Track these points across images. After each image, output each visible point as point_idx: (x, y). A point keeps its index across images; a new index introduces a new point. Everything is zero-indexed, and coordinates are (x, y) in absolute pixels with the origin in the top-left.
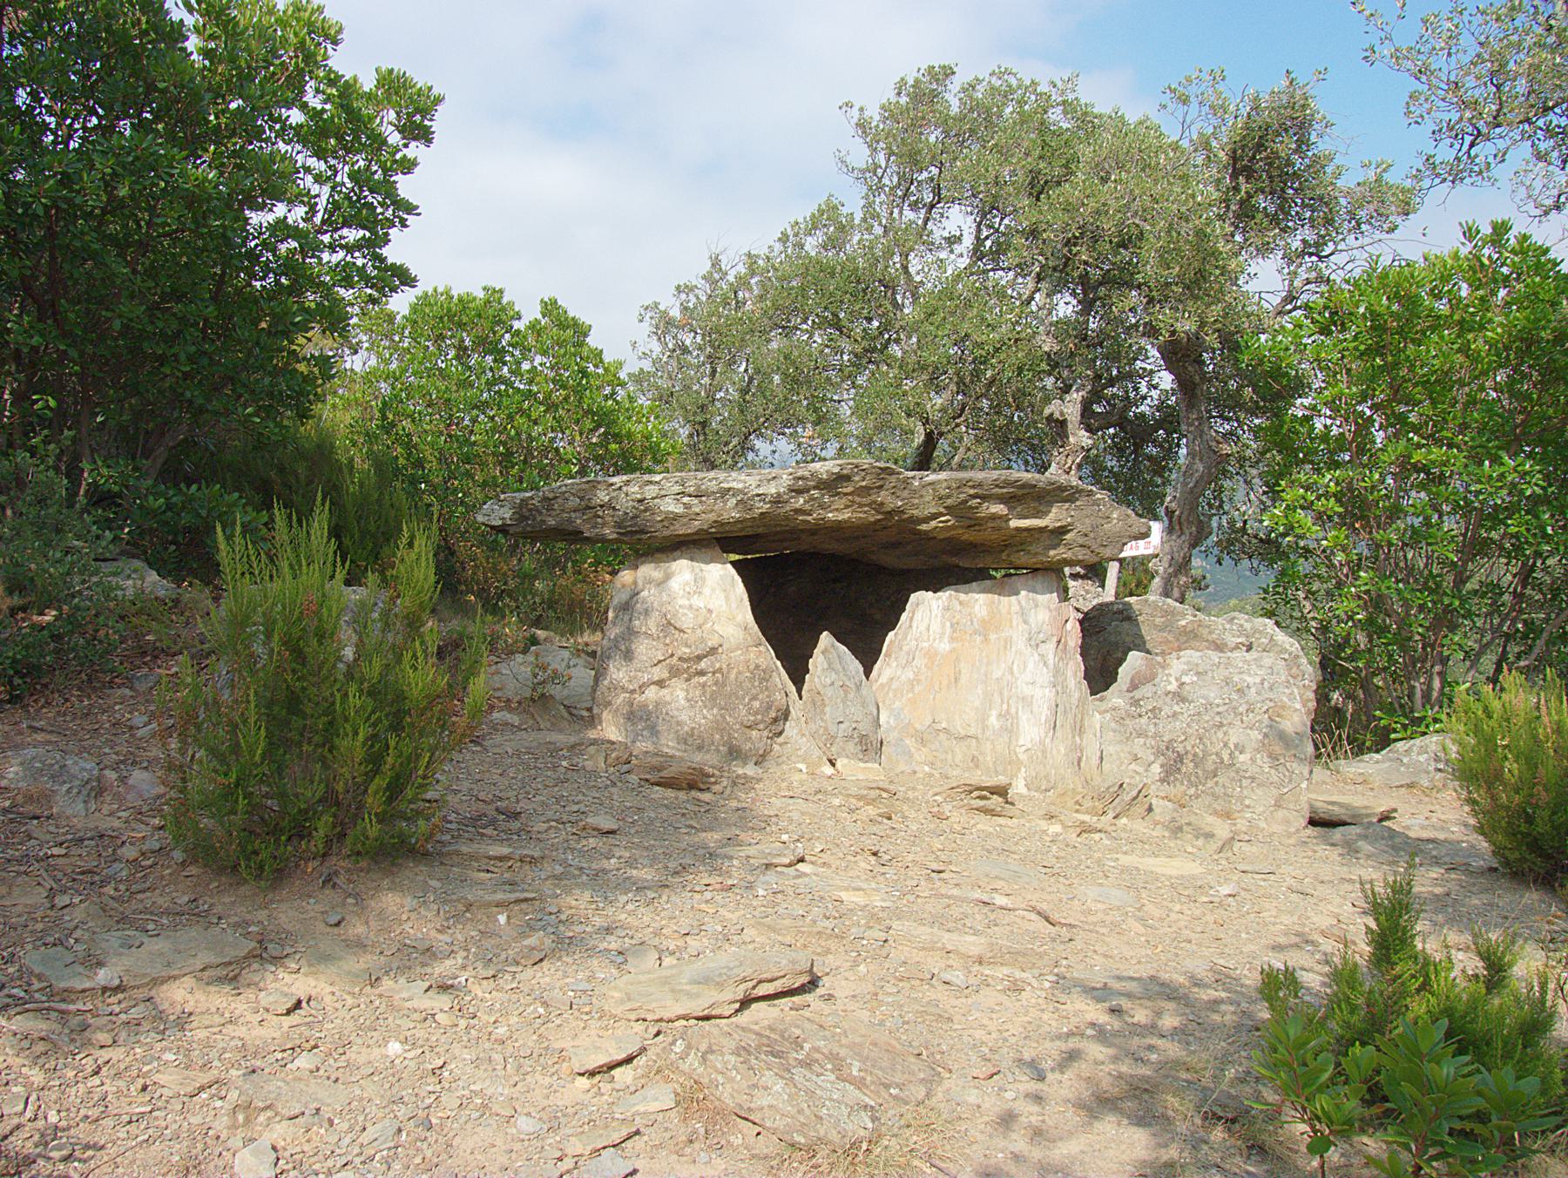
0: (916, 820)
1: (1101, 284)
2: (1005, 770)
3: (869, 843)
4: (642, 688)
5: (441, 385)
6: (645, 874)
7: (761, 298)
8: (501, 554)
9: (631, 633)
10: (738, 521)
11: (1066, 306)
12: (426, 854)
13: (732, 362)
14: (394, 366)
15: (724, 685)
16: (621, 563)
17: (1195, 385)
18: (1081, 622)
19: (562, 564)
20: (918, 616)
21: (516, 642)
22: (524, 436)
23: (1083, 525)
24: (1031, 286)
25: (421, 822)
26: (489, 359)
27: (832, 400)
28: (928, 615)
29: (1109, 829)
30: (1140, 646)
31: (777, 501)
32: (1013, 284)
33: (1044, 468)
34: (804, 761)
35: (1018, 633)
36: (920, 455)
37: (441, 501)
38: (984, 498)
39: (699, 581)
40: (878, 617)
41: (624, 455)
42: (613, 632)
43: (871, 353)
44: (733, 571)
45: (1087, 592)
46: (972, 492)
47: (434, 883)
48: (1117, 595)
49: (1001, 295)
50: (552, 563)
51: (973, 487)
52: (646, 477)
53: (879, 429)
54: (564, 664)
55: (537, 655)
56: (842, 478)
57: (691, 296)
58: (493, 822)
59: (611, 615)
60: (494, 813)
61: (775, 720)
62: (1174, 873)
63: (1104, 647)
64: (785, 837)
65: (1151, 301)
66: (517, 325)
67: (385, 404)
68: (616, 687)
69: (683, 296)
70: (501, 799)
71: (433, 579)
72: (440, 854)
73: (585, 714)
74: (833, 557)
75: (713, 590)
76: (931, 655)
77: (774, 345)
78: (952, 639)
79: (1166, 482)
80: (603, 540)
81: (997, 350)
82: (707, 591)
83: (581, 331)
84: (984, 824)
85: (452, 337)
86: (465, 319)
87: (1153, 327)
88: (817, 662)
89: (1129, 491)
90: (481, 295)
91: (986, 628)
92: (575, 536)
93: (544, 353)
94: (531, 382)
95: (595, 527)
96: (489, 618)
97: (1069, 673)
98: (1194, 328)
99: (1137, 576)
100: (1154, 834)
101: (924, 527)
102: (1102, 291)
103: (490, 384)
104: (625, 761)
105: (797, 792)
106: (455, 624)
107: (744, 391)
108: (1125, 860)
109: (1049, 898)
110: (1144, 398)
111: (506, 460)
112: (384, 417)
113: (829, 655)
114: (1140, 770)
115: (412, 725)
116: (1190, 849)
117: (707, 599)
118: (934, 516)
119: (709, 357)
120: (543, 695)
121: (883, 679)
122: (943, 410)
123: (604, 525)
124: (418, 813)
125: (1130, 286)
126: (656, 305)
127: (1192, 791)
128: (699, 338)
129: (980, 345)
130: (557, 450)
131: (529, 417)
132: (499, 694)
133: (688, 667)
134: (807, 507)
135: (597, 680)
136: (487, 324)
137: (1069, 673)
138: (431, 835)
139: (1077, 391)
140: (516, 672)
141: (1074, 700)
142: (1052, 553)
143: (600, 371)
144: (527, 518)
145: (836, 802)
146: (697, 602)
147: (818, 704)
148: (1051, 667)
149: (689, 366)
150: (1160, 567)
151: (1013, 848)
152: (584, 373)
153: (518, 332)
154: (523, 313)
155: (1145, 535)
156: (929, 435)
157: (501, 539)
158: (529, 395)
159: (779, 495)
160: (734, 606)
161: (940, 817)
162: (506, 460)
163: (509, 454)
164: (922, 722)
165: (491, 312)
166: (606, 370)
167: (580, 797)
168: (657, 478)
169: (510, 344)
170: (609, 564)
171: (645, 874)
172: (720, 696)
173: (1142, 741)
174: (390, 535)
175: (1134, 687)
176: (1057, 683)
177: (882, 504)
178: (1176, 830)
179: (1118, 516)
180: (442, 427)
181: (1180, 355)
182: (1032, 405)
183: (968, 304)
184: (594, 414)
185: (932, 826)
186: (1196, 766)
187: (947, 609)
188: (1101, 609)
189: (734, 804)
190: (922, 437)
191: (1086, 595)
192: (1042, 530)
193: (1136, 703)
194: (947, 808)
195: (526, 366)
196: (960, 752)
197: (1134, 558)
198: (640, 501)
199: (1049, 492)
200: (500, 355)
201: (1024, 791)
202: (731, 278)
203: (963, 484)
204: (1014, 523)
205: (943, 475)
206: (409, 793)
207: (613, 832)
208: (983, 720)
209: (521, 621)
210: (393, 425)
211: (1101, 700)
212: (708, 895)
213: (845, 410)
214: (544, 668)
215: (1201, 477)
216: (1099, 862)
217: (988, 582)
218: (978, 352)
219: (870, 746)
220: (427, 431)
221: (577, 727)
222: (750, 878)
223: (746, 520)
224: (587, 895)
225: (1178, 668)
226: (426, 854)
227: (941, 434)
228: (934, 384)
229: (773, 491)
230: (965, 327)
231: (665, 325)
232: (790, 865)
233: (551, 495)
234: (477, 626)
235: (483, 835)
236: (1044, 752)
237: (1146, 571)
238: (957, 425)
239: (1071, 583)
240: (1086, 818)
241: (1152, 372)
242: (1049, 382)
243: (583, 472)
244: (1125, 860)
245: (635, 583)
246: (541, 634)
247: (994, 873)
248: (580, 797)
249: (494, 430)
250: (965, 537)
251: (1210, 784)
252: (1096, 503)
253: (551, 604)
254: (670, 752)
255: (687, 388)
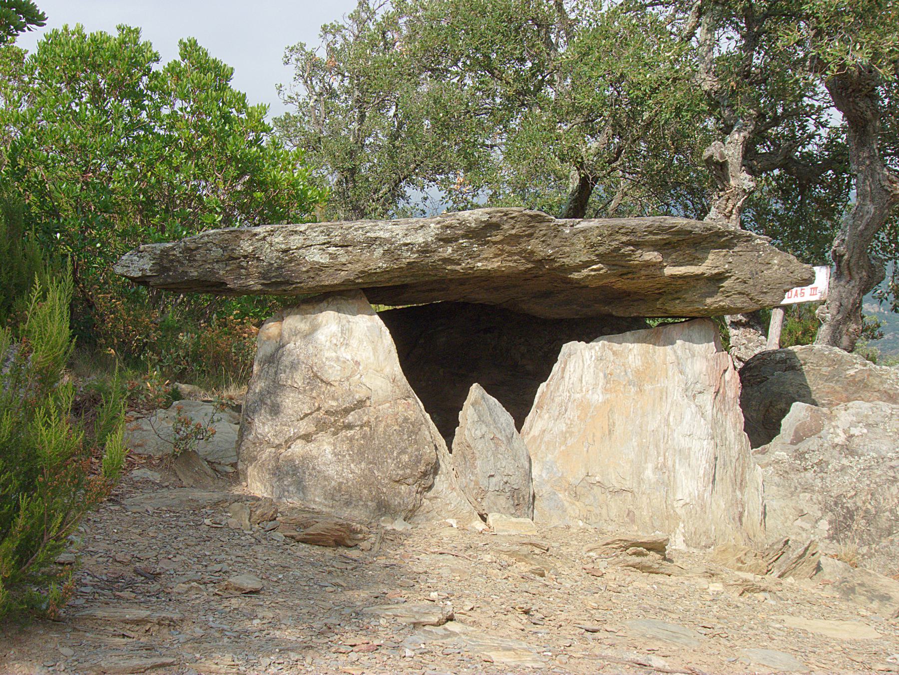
0: (570, 577)
1: (766, 16)
2: (662, 526)
3: (521, 600)
4: (288, 442)
5: (76, 130)
6: (290, 635)
7: (410, 39)
8: (142, 306)
9: (276, 387)
10: (386, 272)
11: (728, 41)
12: (58, 620)
13: (381, 106)
14: (24, 108)
15: (372, 438)
16: (268, 314)
17: (867, 122)
18: (741, 372)
19: (204, 316)
20: (570, 367)
21: (157, 397)
22: (165, 184)
23: (741, 271)
24: (692, 20)
25: (53, 587)
26: (127, 103)
27: (483, 145)
28: (581, 367)
29: (774, 588)
30: (805, 395)
31: (425, 250)
32: (671, 20)
33: (703, 212)
34: (454, 516)
35: (674, 384)
36: (575, 200)
37: (77, 250)
38: (637, 245)
39: (346, 332)
40: (530, 368)
41: (271, 203)
42: (259, 386)
43: (524, 95)
44: (381, 323)
45: (749, 341)
46: (624, 239)
47: (66, 651)
48: (782, 344)
49: (659, 30)
50: (197, 315)
51: (625, 234)
52: (291, 227)
53: (531, 176)
54: (207, 419)
55: (179, 410)
56: (490, 227)
57: (338, 37)
58: (131, 585)
59: (256, 368)
60: (132, 575)
61: (425, 474)
62: (846, 637)
63: (765, 399)
64: (434, 595)
65: (819, 33)
66: (155, 67)
67: (15, 149)
68: (260, 442)
69: (330, 37)
70: (140, 560)
71: (67, 332)
72: (73, 619)
73: (230, 469)
74: (483, 306)
75: (361, 342)
76: (584, 406)
77: (424, 89)
78: (606, 390)
79: (835, 225)
80: (247, 291)
81: (654, 90)
82: (354, 343)
83: (222, 74)
84: (642, 581)
85: (86, 78)
86: (99, 61)
87: (820, 61)
88: (467, 414)
89: (795, 235)
90: (115, 34)
91: (640, 379)
92: (218, 287)
93: (185, 98)
94: (172, 127)
95: (239, 278)
96: (130, 372)
97: (729, 425)
98: (866, 61)
99: (802, 323)
100: (824, 594)
101: (575, 276)
102: (767, 24)
103: (128, 129)
104: (269, 518)
105: (448, 548)
106: (94, 379)
107: (394, 137)
108: (792, 622)
109: (709, 660)
110: (811, 136)
111: (146, 208)
112: (14, 163)
113: (479, 407)
114: (807, 526)
115: (45, 484)
116: (863, 612)
117: (353, 352)
118: (586, 265)
119: (358, 101)
120: (185, 451)
121: (535, 431)
122: (598, 154)
123: (248, 275)
124: (50, 577)
125: (799, 16)
126: (302, 46)
127: (865, 549)
128: (347, 82)
129: (636, 86)
130: (200, 198)
131: (170, 164)
132: (140, 450)
133: (334, 421)
134: (456, 256)
135: (241, 435)
136: (122, 66)
137: (729, 425)
138: (63, 600)
139: (739, 131)
140: (157, 429)
141: (734, 453)
142: (709, 301)
143: (244, 116)
144: (169, 270)
145: (487, 558)
146: (345, 354)
147: (468, 458)
148: (709, 418)
149: (337, 110)
150: (828, 314)
151: (671, 607)
152: (227, 118)
153: (156, 75)
154: (161, 54)
155: (808, 281)
156: (584, 181)
157: (143, 290)
158: (169, 141)
159: (427, 244)
160: (381, 358)
161: (594, 574)
162: (146, 208)
163: (150, 202)
164: (575, 475)
165: (127, 53)
166: (250, 115)
167: (223, 556)
168: (302, 227)
169: (148, 88)
170: (256, 315)
171: (290, 635)
172: (367, 449)
173: (808, 495)
174: (22, 288)
175: (798, 439)
176: (716, 435)
177: (532, 252)
178: (848, 592)
179: (779, 262)
180: (77, 174)
181: (851, 90)
182: (691, 147)
183: (625, 43)
184: (238, 161)
185: (587, 583)
186: (869, 523)
187: (600, 359)
188: (764, 358)
189: (382, 561)
190: (577, 183)
191: (748, 344)
192: (697, 277)
193: (801, 456)
194: (602, 565)
195: (165, 111)
196: (615, 507)
197: (800, 305)
198: (285, 251)
199: (705, 238)
200: (137, 98)
201: (682, 547)
202: (379, 18)
203: (615, 232)
204: (669, 271)
205: (595, 223)
206: (41, 555)
207: (256, 592)
208: (638, 474)
209: (163, 375)
210: (24, 171)
211: (763, 452)
212: (353, 656)
213: (497, 155)
214: (187, 423)
215: (873, 218)
216: (763, 623)
217: (642, 332)
218: (635, 93)
219: (522, 500)
220: (62, 180)
221: (221, 483)
222: (397, 638)
223: (393, 270)
224: (228, 659)
225: (846, 419)
226: (58, 620)
227: (596, 179)
228: (589, 127)
229: (421, 240)
230: (621, 67)
231: (311, 68)
232: (438, 624)
233: (193, 246)
234: (113, 383)
235: (119, 598)
236: (703, 507)
237: (813, 318)
238: (613, 170)
239: (732, 332)
240: (750, 576)
241: (820, 109)
242: (710, 123)
243: (228, 220)
244: (792, 622)
245: (281, 335)
246: (184, 388)
247: (650, 633)
248: (223, 556)
249: (134, 178)
250: (619, 285)
251: (884, 542)
252: (756, 249)
253: (196, 357)
254: (317, 508)
255: (335, 133)
